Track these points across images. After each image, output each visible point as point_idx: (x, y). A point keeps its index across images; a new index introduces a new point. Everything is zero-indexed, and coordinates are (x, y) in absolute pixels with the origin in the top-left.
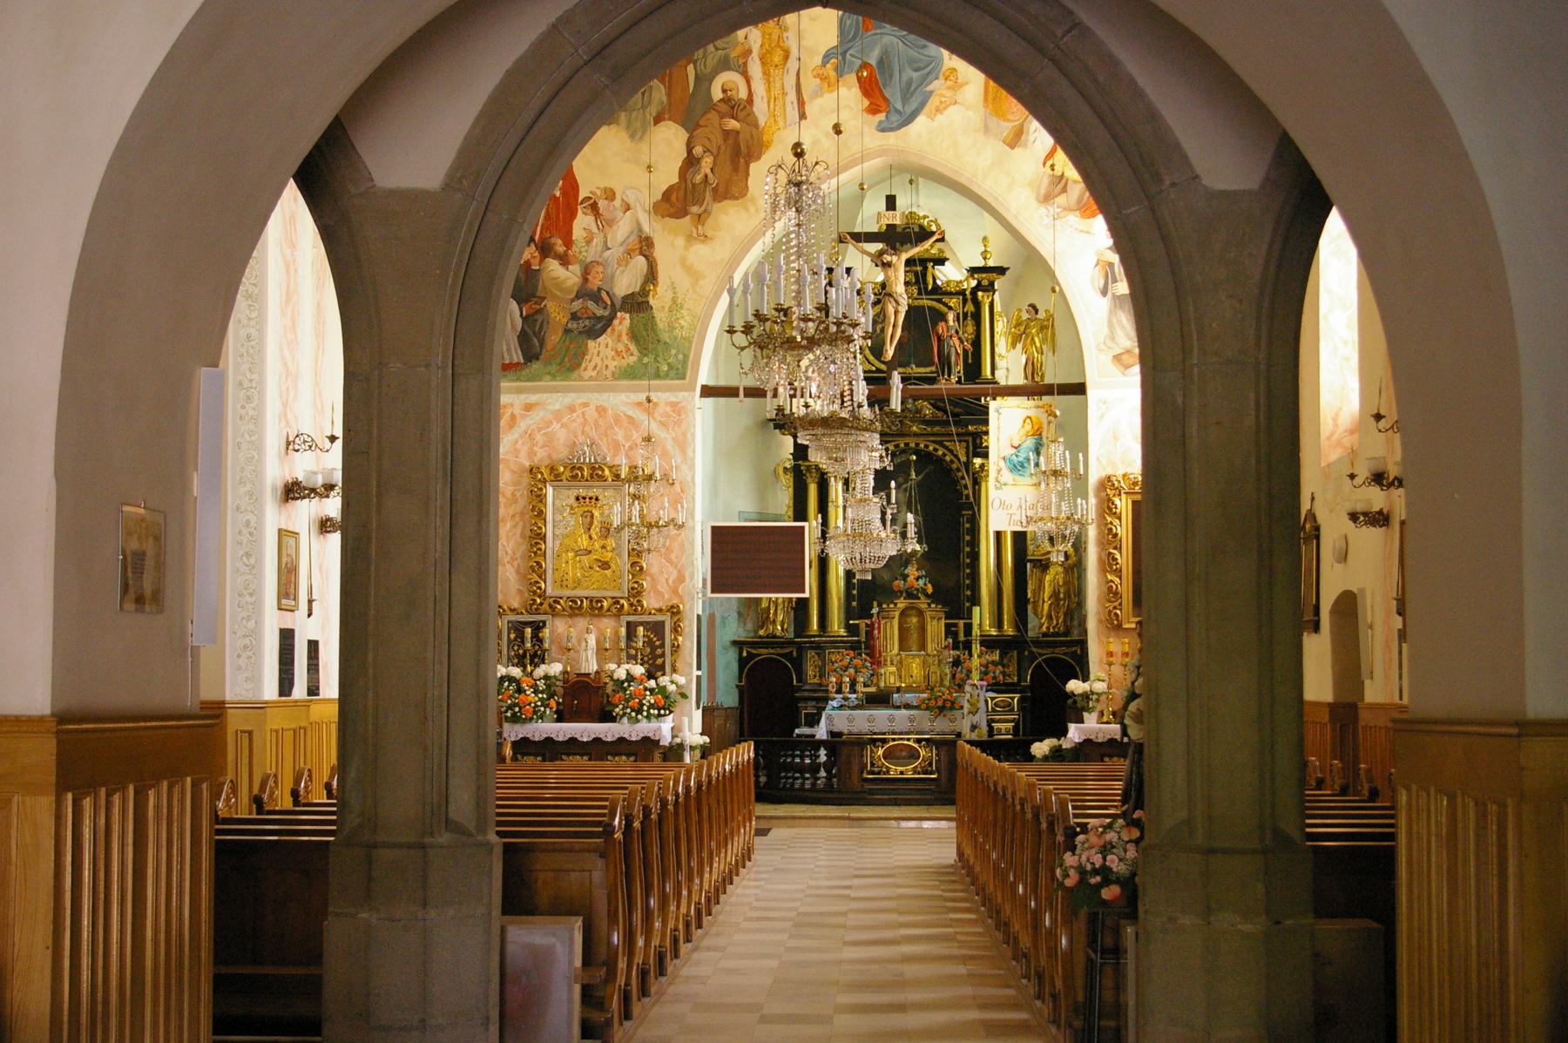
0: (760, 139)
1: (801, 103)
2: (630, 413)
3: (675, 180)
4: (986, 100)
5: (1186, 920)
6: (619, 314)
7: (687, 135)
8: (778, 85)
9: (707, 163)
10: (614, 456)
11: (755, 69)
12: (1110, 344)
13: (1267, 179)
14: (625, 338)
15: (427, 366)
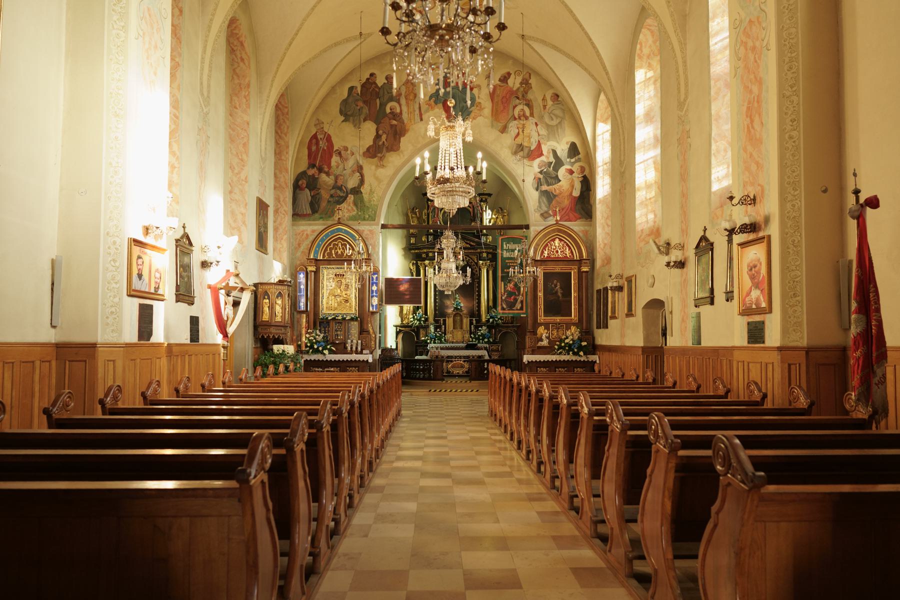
4: (492, 115)
9: (384, 137)
12: (539, 209)
14: (351, 205)
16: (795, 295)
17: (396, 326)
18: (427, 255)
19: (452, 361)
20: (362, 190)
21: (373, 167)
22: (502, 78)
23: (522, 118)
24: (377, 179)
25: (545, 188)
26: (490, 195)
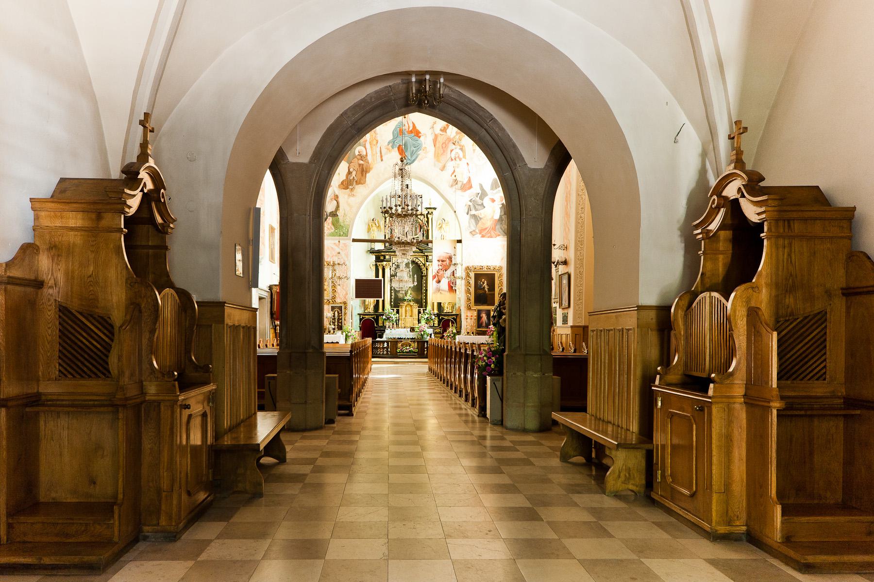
0: (369, 167)
1: (381, 156)
2: (332, 246)
3: (345, 178)
4: (435, 157)
5: (519, 374)
6: (328, 217)
7: (348, 165)
8: (375, 150)
9: (354, 174)
10: (328, 258)
11: (368, 146)
13: (546, 165)
14: (330, 224)
15: (305, 215)
16: (579, 299)
17: (360, 314)
18: (385, 258)
19: (401, 341)
20: (337, 213)
21: (346, 196)
22: (442, 129)
23: (457, 159)
24: (349, 205)
25: (473, 212)
26: (435, 209)
